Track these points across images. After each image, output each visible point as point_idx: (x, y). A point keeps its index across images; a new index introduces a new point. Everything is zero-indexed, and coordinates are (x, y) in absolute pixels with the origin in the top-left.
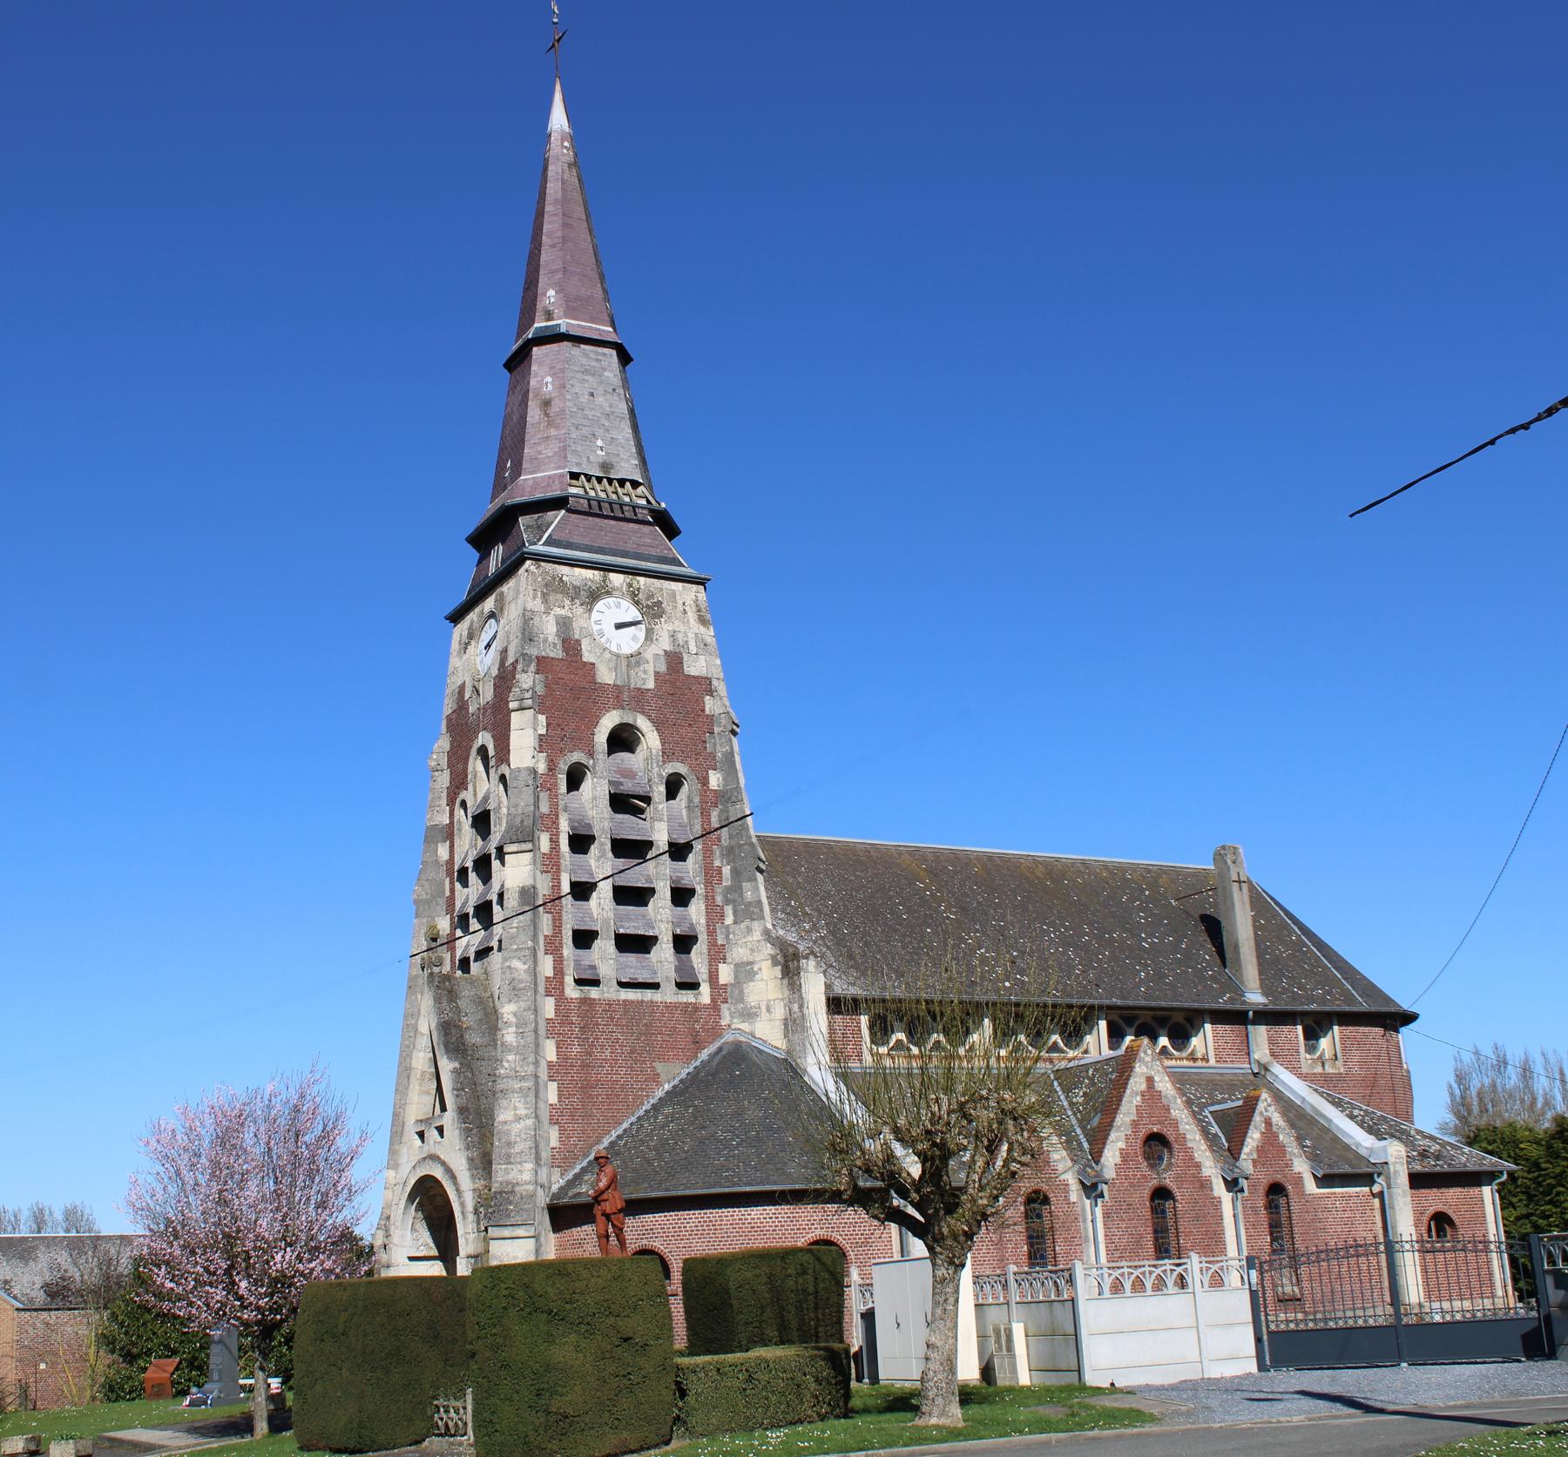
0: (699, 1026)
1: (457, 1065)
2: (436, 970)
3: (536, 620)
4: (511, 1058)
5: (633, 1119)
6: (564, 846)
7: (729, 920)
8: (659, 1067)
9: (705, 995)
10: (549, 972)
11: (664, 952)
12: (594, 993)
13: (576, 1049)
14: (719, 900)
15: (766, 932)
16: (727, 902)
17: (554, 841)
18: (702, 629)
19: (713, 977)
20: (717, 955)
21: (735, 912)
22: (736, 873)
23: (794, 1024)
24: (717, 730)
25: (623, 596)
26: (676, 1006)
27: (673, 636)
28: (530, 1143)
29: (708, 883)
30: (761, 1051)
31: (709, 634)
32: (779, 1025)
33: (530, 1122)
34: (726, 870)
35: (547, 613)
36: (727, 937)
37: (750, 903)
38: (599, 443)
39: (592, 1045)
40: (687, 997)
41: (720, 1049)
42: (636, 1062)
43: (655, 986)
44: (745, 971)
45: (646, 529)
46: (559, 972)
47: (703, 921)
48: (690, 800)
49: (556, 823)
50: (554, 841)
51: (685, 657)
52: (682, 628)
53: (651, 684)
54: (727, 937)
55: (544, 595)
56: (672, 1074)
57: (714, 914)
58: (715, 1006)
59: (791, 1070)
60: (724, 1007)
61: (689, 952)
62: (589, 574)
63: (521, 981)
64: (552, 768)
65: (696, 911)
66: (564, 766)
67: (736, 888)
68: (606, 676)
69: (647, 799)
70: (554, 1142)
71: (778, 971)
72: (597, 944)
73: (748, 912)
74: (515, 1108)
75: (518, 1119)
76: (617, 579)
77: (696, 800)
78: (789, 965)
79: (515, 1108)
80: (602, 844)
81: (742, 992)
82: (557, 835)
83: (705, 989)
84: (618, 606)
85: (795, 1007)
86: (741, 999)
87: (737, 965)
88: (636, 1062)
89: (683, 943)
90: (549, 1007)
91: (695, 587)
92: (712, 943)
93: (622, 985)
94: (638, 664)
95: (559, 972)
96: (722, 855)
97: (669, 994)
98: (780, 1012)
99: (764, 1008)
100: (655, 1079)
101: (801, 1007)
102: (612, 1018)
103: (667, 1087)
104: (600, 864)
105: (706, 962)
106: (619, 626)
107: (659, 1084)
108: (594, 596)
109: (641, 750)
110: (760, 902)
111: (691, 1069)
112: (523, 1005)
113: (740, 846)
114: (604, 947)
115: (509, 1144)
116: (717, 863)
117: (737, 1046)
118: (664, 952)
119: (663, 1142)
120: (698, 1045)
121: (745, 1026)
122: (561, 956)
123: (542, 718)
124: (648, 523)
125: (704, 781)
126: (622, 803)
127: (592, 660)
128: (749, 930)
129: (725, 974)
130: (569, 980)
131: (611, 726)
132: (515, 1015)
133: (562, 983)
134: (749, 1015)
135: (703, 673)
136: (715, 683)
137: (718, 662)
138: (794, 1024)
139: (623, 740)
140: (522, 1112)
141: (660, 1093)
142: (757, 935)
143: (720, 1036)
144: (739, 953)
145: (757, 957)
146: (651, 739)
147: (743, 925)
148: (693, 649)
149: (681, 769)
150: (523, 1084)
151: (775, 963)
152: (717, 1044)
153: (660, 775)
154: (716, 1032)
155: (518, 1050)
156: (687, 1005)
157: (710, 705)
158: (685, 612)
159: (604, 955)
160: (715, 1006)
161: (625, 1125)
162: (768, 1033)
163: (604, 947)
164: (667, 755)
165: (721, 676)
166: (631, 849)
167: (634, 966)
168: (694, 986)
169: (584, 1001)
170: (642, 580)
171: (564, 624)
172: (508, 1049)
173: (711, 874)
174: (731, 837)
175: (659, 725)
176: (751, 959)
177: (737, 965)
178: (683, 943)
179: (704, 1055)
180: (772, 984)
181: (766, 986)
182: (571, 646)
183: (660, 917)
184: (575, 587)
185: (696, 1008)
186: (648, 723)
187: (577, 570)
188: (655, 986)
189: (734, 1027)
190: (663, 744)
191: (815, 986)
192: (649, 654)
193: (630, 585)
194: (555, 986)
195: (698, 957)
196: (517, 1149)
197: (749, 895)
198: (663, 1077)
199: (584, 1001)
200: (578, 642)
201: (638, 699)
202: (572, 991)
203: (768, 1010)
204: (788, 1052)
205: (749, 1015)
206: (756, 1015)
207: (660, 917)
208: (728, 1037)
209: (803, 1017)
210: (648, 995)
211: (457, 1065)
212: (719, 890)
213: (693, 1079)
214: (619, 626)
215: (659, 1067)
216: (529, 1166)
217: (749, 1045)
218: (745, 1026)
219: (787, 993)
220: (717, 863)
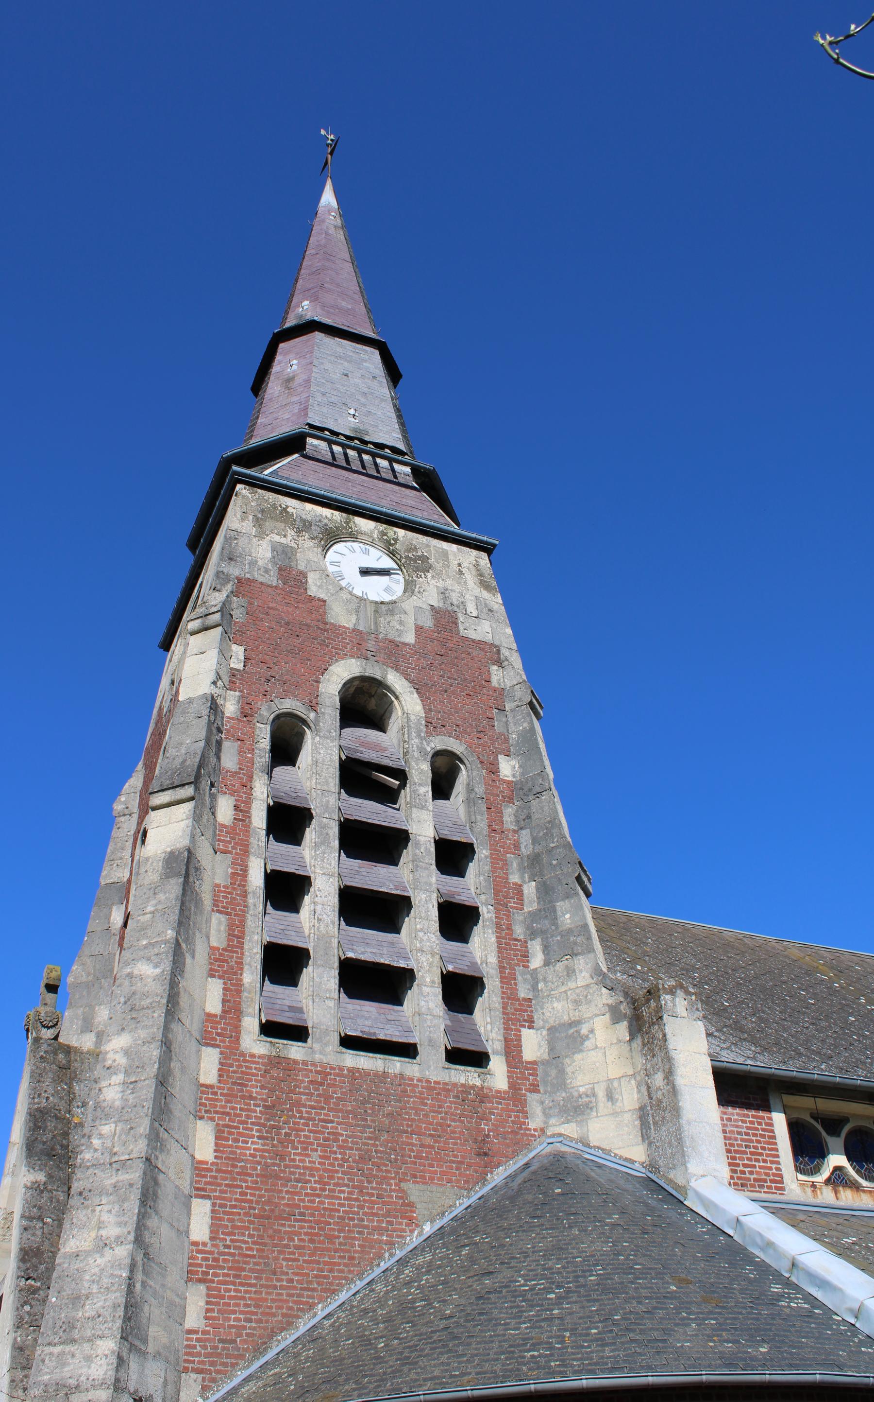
0: (486, 1132)
1: (41, 1177)
2: (47, 1034)
3: (242, 542)
4: (107, 1129)
5: (360, 1284)
6: (259, 819)
7: (537, 961)
8: (414, 1191)
9: (498, 1075)
10: (213, 1004)
11: (425, 999)
12: (295, 1050)
13: (254, 1145)
14: (519, 931)
15: (597, 971)
16: (533, 934)
17: (242, 811)
18: (485, 594)
19: (512, 1050)
20: (519, 1014)
21: (546, 949)
22: (545, 891)
23: (658, 1112)
24: (508, 706)
25: (372, 544)
26: (446, 1088)
27: (444, 593)
28: (118, 1297)
29: (500, 905)
30: (600, 1166)
31: (496, 601)
32: (630, 1122)
33: (123, 1252)
34: (530, 889)
35: (261, 535)
36: (534, 988)
37: (570, 931)
38: (352, 412)
39: (286, 1141)
40: (466, 1076)
41: (527, 1165)
42: (370, 1178)
43: (407, 1050)
44: (567, 1038)
45: (408, 492)
46: (232, 1008)
47: (493, 959)
48: (470, 789)
49: (247, 786)
50: (242, 811)
51: (461, 618)
52: (457, 587)
53: (410, 638)
54: (534, 988)
55: (257, 519)
56: (437, 1205)
57: (512, 953)
58: (515, 1096)
59: (660, 1195)
60: (532, 1099)
61: (470, 1012)
62: (326, 512)
63: (145, 995)
64: (247, 713)
65: (481, 950)
66: (266, 712)
67: (547, 911)
68: (340, 615)
69: (401, 775)
70: (194, 1318)
71: (623, 1029)
72: (308, 975)
73: (562, 948)
74: (100, 1225)
75: (103, 1245)
76: (364, 525)
77: (480, 790)
78: (642, 1020)
79: (100, 1225)
80: (324, 827)
81: (562, 1072)
82: (249, 801)
83: (498, 1065)
84: (367, 552)
85: (658, 1079)
86: (561, 1083)
87: (552, 1030)
88: (370, 1178)
89: (460, 991)
90: (208, 1065)
91: (474, 553)
92: (509, 995)
93: (349, 1042)
94: (391, 612)
95: (232, 1008)
96: (522, 869)
97: (431, 1066)
98: (630, 1097)
99: (601, 1094)
100: (407, 1213)
101: (669, 1075)
102: (327, 1098)
103: (428, 1229)
104: (320, 859)
105: (499, 1024)
106: (365, 572)
107: (413, 1223)
108: (331, 537)
109: (395, 723)
110: (585, 926)
111: (474, 1198)
112: (143, 1034)
113: (550, 851)
114: (320, 981)
115: (77, 1300)
116: (515, 878)
117: (558, 1158)
118: (425, 999)
119: (405, 1307)
120: (486, 1157)
121: (570, 1129)
122: (239, 984)
123: (238, 651)
124: (413, 488)
125: (493, 769)
126: (357, 776)
127: (322, 596)
128: (570, 972)
129: (533, 1045)
130: (251, 1024)
131: (346, 676)
132: (127, 1052)
133: (237, 1028)
134: (578, 1108)
135: (489, 638)
136: (505, 652)
137: (509, 631)
138: (658, 1112)
139: (363, 706)
140: (111, 1231)
141: (414, 1240)
142: (584, 977)
143: (527, 1146)
144: (555, 1010)
145: (586, 1011)
146: (408, 704)
147: (560, 967)
148: (471, 608)
149: (457, 747)
150: (124, 1177)
151: (616, 1016)
152: (521, 1161)
153: (422, 750)
154: (520, 1138)
155: (122, 1115)
156: (466, 1089)
157: (496, 675)
158: (461, 573)
159: (317, 995)
160: (515, 1096)
161: (343, 1296)
162: (613, 1136)
163: (320, 981)
164: (432, 726)
165: (514, 646)
166: (370, 842)
167: (370, 1017)
168: (476, 1059)
169: (276, 1062)
170: (401, 532)
171: (284, 558)
172: (103, 1112)
173: (506, 896)
174: (535, 840)
175: (419, 688)
176: (575, 1016)
177: (552, 1030)
178: (460, 991)
179: (498, 1176)
180: (612, 1054)
181: (604, 1057)
182: (292, 579)
183: (419, 945)
184: (304, 521)
185: (483, 1095)
186: (406, 683)
187: (309, 506)
188: (407, 1050)
189: (551, 1129)
190: (428, 711)
191: (692, 1048)
192: (409, 605)
193: (383, 534)
194: (221, 1031)
195: (486, 1021)
196: (89, 1310)
197: (567, 919)
198: (420, 1211)
199: (276, 1062)
200: (304, 575)
201: (393, 651)
202: (254, 1043)
203: (610, 1096)
204: (652, 1166)
205: (578, 1108)
206: (588, 1107)
207: (419, 945)
208: (540, 1149)
209: (674, 1091)
210: (396, 1065)
211: (41, 1177)
212: (518, 917)
213: (472, 1211)
214: (365, 572)
215: (414, 1191)
216: (108, 1346)
217: (579, 1157)
218: (570, 1129)
219: (640, 1061)
220: (515, 878)
